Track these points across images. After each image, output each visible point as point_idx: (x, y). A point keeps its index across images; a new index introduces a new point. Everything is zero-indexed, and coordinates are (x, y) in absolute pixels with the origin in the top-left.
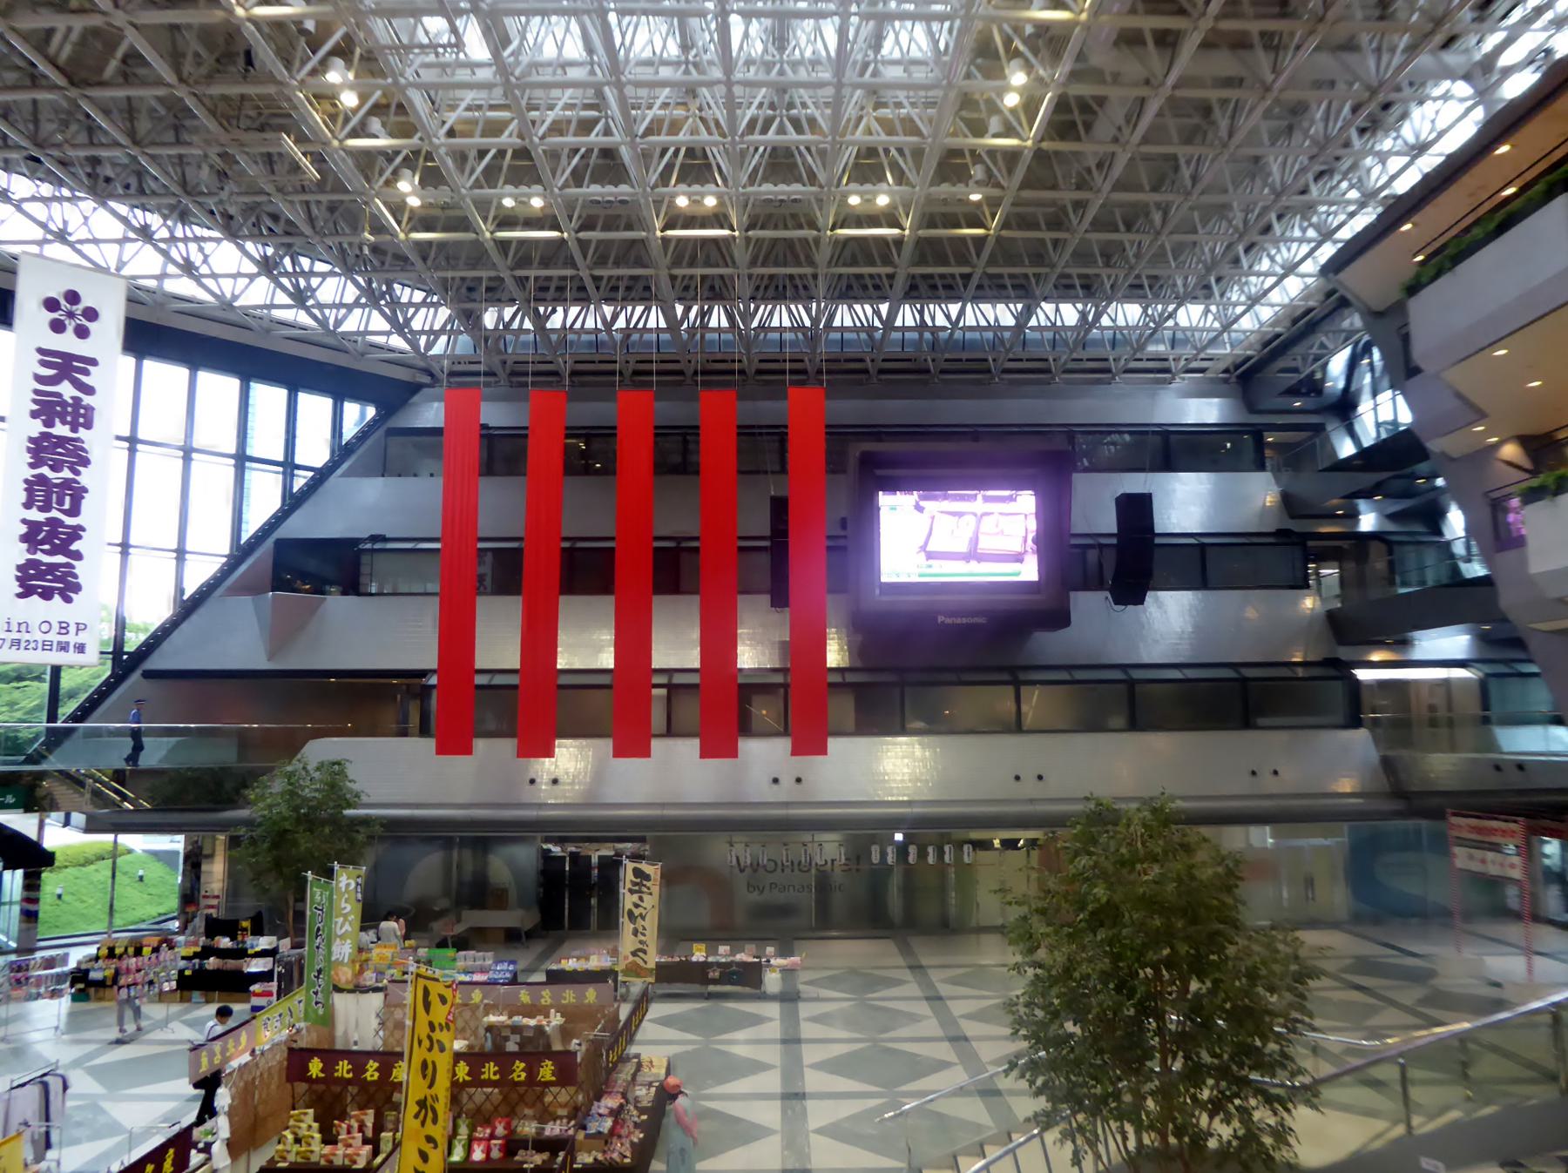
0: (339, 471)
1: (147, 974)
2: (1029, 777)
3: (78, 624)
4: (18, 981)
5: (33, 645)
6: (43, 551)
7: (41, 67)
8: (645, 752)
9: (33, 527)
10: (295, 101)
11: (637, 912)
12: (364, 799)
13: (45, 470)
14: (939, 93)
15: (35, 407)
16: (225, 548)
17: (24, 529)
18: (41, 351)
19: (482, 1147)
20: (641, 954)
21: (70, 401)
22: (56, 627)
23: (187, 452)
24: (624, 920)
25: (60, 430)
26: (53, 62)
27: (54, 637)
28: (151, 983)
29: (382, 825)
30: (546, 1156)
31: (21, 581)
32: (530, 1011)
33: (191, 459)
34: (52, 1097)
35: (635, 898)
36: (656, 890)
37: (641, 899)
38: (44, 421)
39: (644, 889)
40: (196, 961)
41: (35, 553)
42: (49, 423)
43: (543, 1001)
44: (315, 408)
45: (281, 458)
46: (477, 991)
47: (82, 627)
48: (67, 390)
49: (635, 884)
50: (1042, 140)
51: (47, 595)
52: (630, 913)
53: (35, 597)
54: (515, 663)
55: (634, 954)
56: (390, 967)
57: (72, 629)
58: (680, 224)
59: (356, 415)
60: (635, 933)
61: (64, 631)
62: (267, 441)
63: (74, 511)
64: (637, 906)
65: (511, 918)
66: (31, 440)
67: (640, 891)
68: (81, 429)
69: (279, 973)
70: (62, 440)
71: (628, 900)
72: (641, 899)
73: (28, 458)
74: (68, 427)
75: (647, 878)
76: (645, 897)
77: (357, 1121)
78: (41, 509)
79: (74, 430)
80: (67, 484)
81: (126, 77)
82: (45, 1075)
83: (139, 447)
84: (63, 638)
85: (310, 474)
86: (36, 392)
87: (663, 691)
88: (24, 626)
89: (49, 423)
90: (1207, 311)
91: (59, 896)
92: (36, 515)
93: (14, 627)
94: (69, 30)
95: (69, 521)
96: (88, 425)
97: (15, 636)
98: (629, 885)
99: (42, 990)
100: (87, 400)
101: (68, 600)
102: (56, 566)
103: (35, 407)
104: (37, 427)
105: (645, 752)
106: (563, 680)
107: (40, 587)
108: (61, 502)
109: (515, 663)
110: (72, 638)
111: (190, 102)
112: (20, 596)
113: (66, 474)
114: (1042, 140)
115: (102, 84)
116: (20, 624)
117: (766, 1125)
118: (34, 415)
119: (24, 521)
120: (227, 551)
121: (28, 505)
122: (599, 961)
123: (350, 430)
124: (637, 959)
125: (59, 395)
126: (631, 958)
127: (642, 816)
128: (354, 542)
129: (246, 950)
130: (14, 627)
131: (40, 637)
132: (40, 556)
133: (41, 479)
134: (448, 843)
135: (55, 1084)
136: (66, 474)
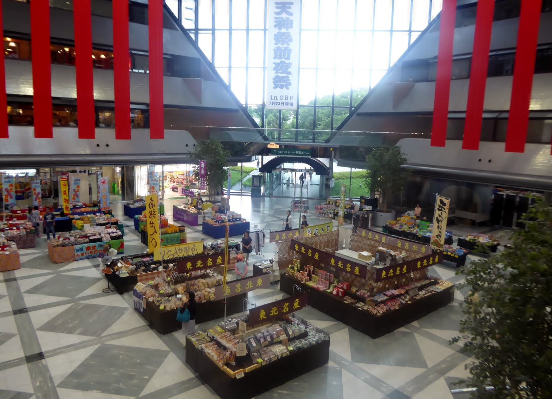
0: (429, 30)
1: (324, 211)
3: (290, 96)
4: (296, 206)
5: (278, 103)
6: (280, 73)
8: (443, 145)
9: (277, 65)
11: (440, 219)
12: (408, 162)
13: (280, 45)
15: (275, 24)
17: (274, 66)
18: (276, 3)
19: (336, 290)
20: (439, 237)
21: (286, 19)
22: (284, 98)
24: (435, 221)
25: (283, 30)
27: (284, 101)
28: (325, 213)
29: (412, 172)
30: (353, 301)
31: (275, 83)
32: (395, 248)
33: (214, 33)
34: (260, 238)
35: (440, 212)
36: (447, 211)
37: (441, 213)
38: (278, 28)
39: (443, 210)
40: (349, 210)
41: (278, 74)
42: (280, 29)
43: (405, 247)
45: (211, 28)
46: (384, 237)
47: (292, 97)
48: (284, 15)
49: (440, 206)
51: (282, 87)
52: (437, 218)
53: (278, 88)
54: (507, 107)
55: (437, 236)
56: (405, 224)
57: (289, 98)
60: (438, 227)
61: (287, 99)
63: (288, 58)
64: (440, 216)
65: (478, 217)
66: (275, 35)
67: (441, 210)
68: (289, 29)
69: (354, 218)
70: (284, 34)
71: (437, 213)
72: (441, 213)
73: (274, 42)
74: (285, 29)
75: (445, 205)
76: (443, 213)
77: (308, 268)
78: (278, 59)
79: (287, 29)
80: (286, 48)
82: (259, 231)
84: (287, 101)
86: (276, 18)
88: (276, 98)
89: (280, 29)
91: (360, 186)
92: (278, 61)
93: (273, 98)
95: (287, 62)
96: (291, 27)
97: (273, 101)
98: (437, 207)
99: (302, 210)
100: (291, 18)
101: (288, 88)
102: (283, 77)
103: (275, 24)
104: (276, 31)
105: (443, 145)
106: (531, 115)
107: (279, 84)
108: (284, 55)
109: (507, 107)
110: (289, 101)
112: (274, 88)
113: (286, 45)
116: (274, 97)
118: (275, 26)
119: (274, 63)
121: (275, 58)
122: (483, 240)
124: (438, 239)
125: (282, 18)
126: (436, 238)
127: (528, 180)
129: (362, 209)
130: (273, 98)
131: (280, 101)
132: (279, 74)
133: (278, 48)
134: (457, 183)
135: (261, 235)
136: (286, 45)
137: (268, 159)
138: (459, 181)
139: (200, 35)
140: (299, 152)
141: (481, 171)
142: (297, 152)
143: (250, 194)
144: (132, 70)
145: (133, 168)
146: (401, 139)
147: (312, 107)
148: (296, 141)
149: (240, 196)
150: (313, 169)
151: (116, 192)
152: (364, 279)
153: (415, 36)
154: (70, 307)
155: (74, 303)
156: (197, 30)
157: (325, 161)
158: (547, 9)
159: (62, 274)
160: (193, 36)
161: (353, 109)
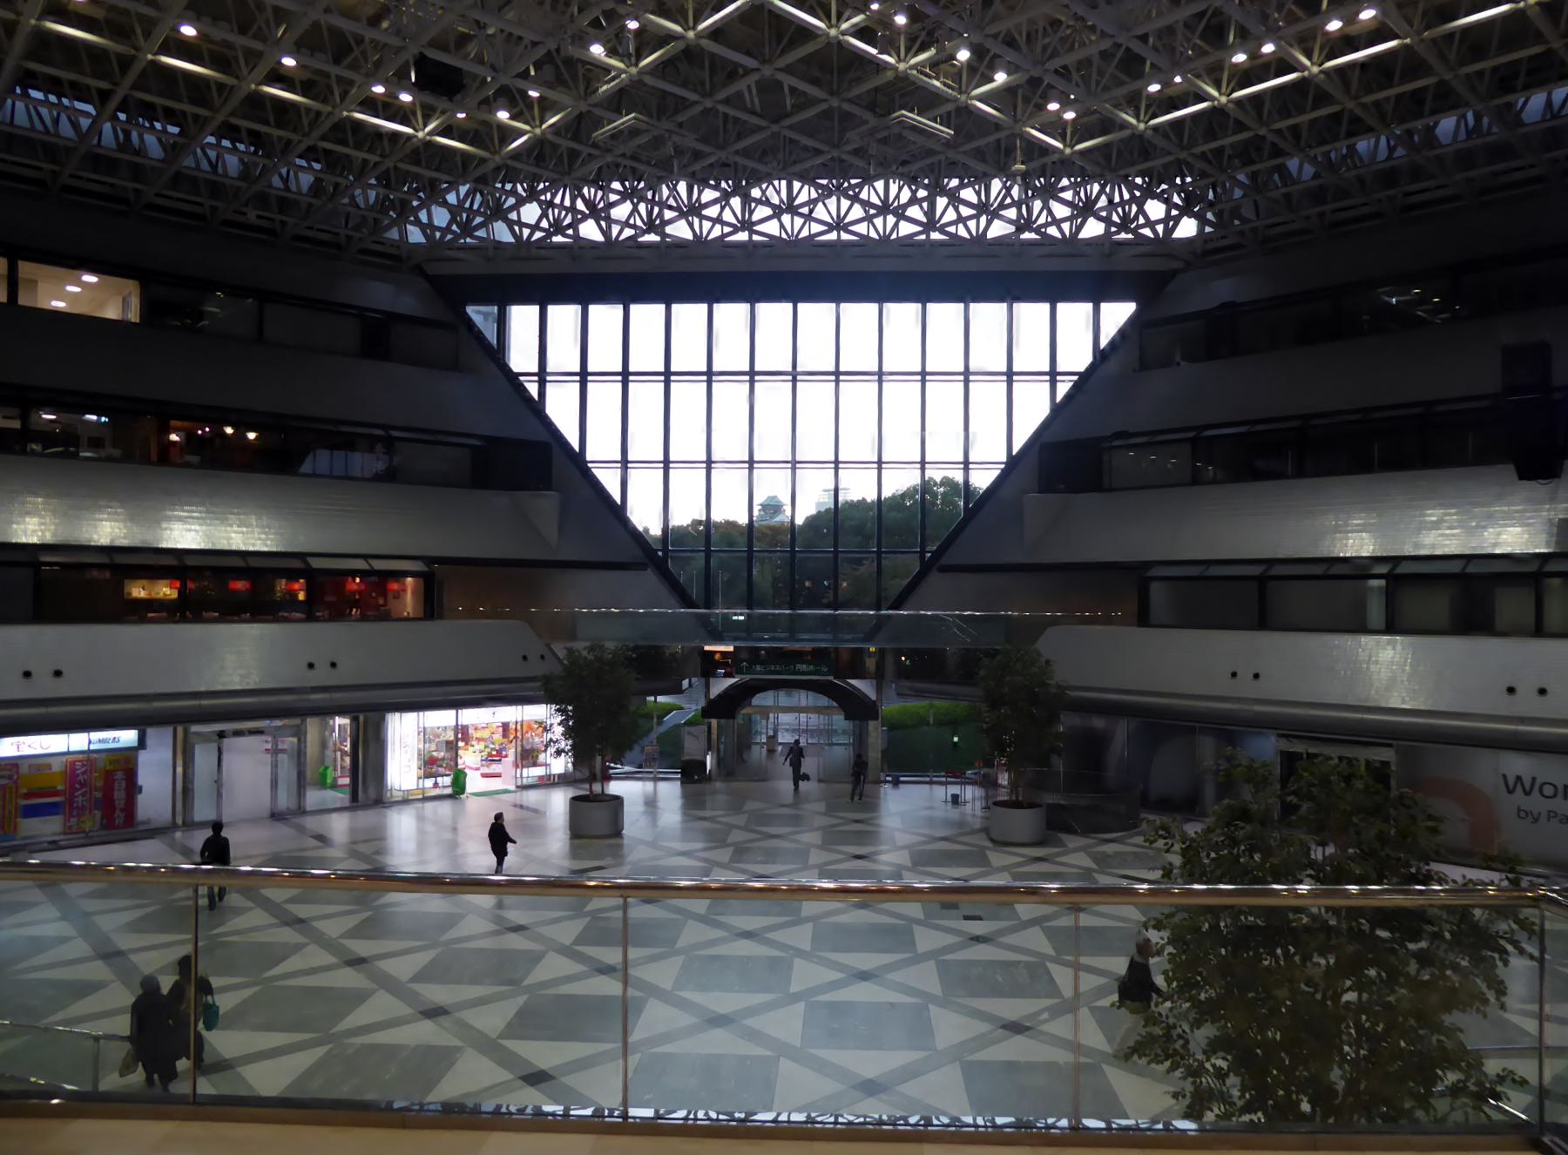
2: (1526, 689)
7: (641, 142)
10: (912, 78)
14: (220, 170)
16: (1003, 457)
23: (1010, 375)
26: (754, 113)
44: (1075, 314)
50: (647, 73)
58: (1272, 71)
59: (1117, 314)
62: (1032, 356)
81: (798, 108)
83: (971, 378)
85: (1076, 378)
87: (1382, 582)
90: (635, 210)
94: (749, 87)
111: (846, 107)
114: (647, 73)
115: (787, 116)
117: (561, 957)
120: (1004, 460)
123: (1108, 332)
128: (1099, 440)
137: (720, 685)
138: (1197, 725)
139: (550, 388)
140: (803, 667)
141: (1238, 700)
142: (799, 666)
143: (679, 776)
144: (1373, 930)
145: (383, 719)
146: (1049, 629)
147: (788, 513)
148: (792, 638)
149: (927, 786)
150: (835, 704)
151: (329, 781)
152: (1357, 146)
153: (1063, 389)
154: (328, 1052)
155: (330, 1046)
156: (542, 375)
157: (864, 686)
158: (1475, 136)
159: (276, 984)
160: (533, 389)
161: (929, 555)
